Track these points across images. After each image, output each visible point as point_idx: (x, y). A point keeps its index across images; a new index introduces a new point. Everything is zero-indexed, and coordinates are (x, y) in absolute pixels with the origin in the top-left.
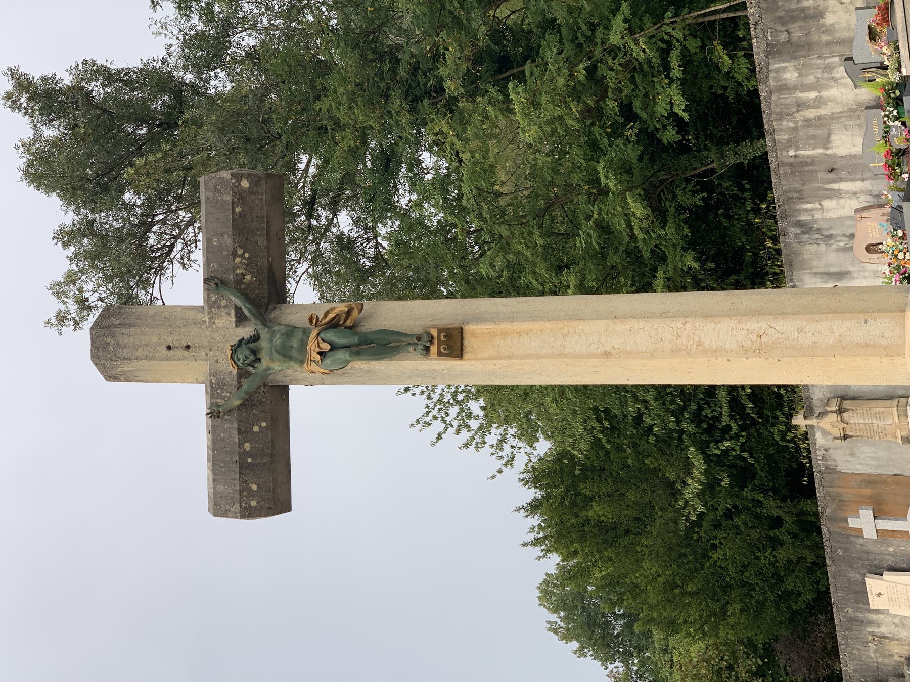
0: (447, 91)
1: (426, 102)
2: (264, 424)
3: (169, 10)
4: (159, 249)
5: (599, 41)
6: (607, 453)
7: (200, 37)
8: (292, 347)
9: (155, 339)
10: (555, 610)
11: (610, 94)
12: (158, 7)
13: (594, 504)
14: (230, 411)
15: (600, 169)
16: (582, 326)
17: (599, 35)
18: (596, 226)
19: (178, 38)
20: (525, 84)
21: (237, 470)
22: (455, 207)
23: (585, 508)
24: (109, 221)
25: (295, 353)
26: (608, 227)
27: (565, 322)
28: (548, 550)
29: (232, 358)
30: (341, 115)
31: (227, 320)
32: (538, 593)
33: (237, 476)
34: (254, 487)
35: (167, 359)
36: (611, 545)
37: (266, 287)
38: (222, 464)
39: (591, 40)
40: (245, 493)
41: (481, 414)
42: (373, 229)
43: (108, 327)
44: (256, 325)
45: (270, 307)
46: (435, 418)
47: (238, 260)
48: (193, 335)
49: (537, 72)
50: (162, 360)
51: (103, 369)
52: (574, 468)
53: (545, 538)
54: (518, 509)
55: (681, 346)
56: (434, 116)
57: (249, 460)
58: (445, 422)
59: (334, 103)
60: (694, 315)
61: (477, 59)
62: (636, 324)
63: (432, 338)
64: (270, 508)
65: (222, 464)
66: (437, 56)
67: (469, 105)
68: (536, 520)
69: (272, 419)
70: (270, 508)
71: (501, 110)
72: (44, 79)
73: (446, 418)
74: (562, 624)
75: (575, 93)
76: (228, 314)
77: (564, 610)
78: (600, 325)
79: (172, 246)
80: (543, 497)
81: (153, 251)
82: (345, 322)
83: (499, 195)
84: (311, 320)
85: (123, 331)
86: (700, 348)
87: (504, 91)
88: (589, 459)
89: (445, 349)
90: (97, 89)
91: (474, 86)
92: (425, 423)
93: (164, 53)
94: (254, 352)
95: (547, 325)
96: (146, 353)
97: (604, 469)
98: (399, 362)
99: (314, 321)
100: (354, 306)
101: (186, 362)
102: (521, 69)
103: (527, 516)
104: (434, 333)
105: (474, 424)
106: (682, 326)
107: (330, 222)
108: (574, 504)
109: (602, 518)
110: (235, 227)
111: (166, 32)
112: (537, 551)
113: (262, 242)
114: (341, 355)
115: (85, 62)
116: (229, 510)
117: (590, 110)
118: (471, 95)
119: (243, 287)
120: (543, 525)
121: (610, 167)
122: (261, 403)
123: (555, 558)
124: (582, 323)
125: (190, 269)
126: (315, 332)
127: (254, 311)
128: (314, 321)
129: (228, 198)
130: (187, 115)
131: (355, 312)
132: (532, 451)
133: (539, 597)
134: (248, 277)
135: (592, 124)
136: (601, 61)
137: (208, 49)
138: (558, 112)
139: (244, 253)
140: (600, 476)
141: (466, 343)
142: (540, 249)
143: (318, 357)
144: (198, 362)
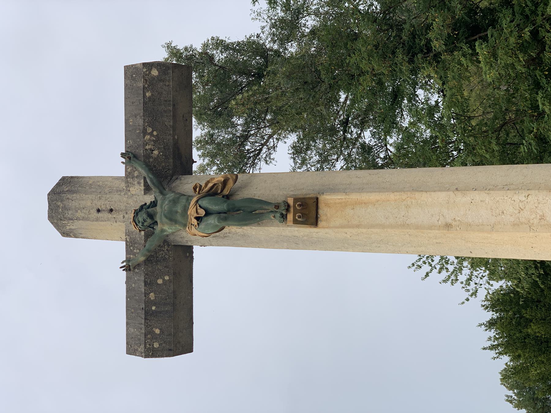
0: (434, 48)
1: (420, 56)
2: (167, 278)
3: (263, 4)
4: (253, 152)
5: (540, 13)
6: (542, 291)
7: (282, 20)
8: (177, 212)
9: (89, 204)
10: (511, 388)
11: (547, 48)
12: (256, 3)
13: (532, 324)
14: (139, 265)
15: (539, 99)
16: (424, 197)
17: (540, 9)
18: (535, 137)
19: (267, 22)
20: (487, 42)
21: (143, 316)
22: (439, 126)
23: (526, 326)
24: (223, 136)
25: (179, 217)
26: (545, 139)
27: (409, 193)
28: (500, 353)
29: (134, 221)
30: (364, 66)
31: (138, 189)
32: (500, 377)
33: (143, 321)
34: (157, 331)
35: (97, 220)
36: (544, 353)
37: (171, 160)
38: (133, 310)
39: (534, 12)
40: (149, 336)
41: (456, 261)
42: (385, 139)
43: (59, 193)
44: (155, 192)
45: (174, 178)
46: (424, 263)
47: (147, 137)
48: (116, 200)
49: (496, 34)
50: (93, 221)
51: (58, 227)
52: (519, 299)
53: (498, 345)
54: (480, 325)
55: (523, 220)
56: (424, 65)
57: (154, 308)
58: (431, 265)
59: (361, 58)
60: (538, 188)
61: (456, 26)
62: (477, 196)
63: (289, 206)
64: (170, 350)
65: (133, 310)
66: (428, 27)
67: (449, 57)
68: (492, 333)
69: (174, 274)
70: (170, 350)
71: (471, 60)
72: (186, 49)
73: (432, 263)
74: (516, 398)
75: (523, 47)
76: (139, 183)
77: (517, 389)
78: (442, 196)
79: (261, 150)
80: (498, 318)
81: (249, 153)
82: (222, 191)
83: (470, 118)
84: (195, 188)
85: (69, 196)
86: (543, 222)
87: (473, 47)
88: (530, 294)
89: (299, 217)
90: (219, 56)
91: (454, 45)
92: (418, 266)
93: (259, 31)
94: (151, 216)
95: (392, 196)
96: (83, 215)
97: (540, 302)
98: (266, 228)
99: (198, 190)
100: (229, 176)
101: (109, 223)
102: (486, 33)
103: (486, 330)
104: (291, 202)
105: (451, 268)
106: (524, 199)
107: (359, 136)
108: (519, 324)
109: (537, 334)
110: (145, 110)
111: (260, 18)
112: (493, 353)
113: (169, 123)
114: (212, 220)
115: (213, 38)
116: (137, 350)
117: (533, 59)
118: (451, 51)
119: (151, 160)
120: (497, 336)
121: (546, 97)
122: (164, 259)
123: (506, 359)
124: (424, 194)
125: (271, 164)
126: (195, 199)
127: (155, 181)
128: (198, 190)
129: (141, 84)
130: (269, 69)
131: (231, 182)
132: (490, 287)
133: (501, 379)
134: (156, 152)
135: (535, 69)
136: (541, 27)
137: (287, 28)
138: (510, 61)
139: (153, 131)
140: (537, 306)
141: (321, 212)
142: (496, 154)
143: (195, 222)
144: (119, 223)
